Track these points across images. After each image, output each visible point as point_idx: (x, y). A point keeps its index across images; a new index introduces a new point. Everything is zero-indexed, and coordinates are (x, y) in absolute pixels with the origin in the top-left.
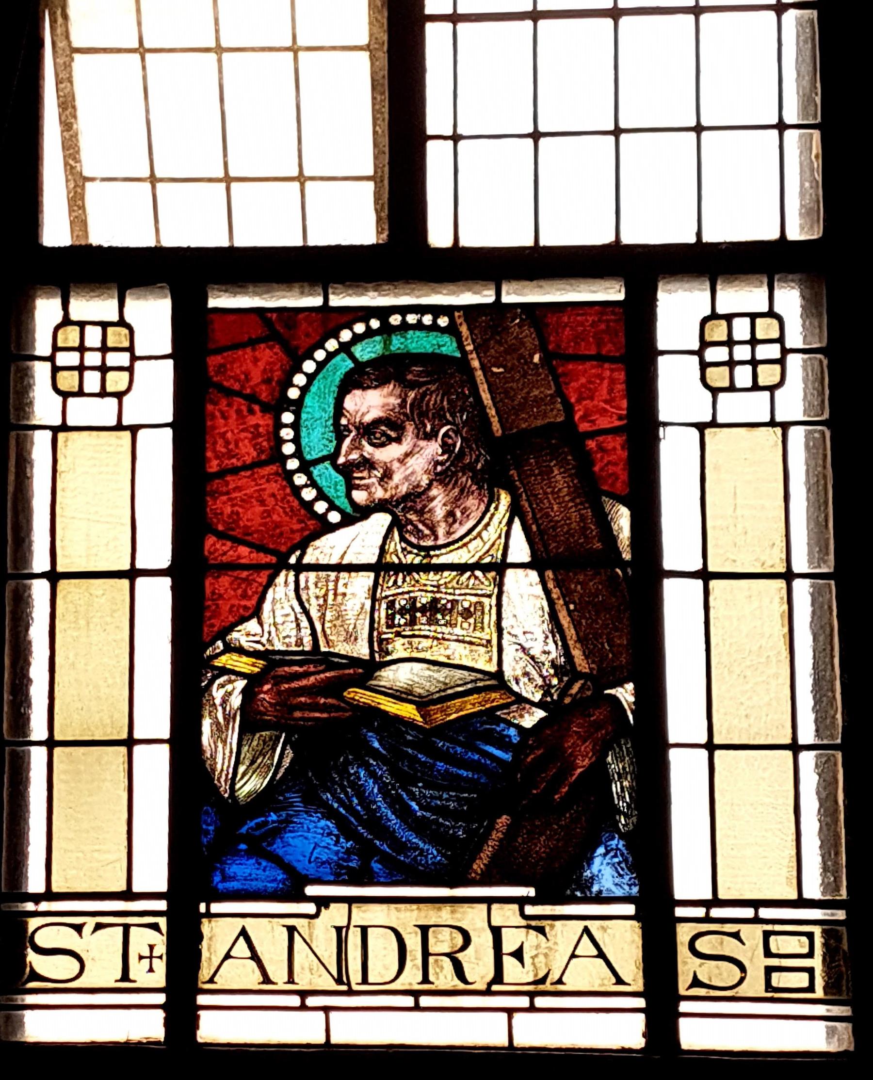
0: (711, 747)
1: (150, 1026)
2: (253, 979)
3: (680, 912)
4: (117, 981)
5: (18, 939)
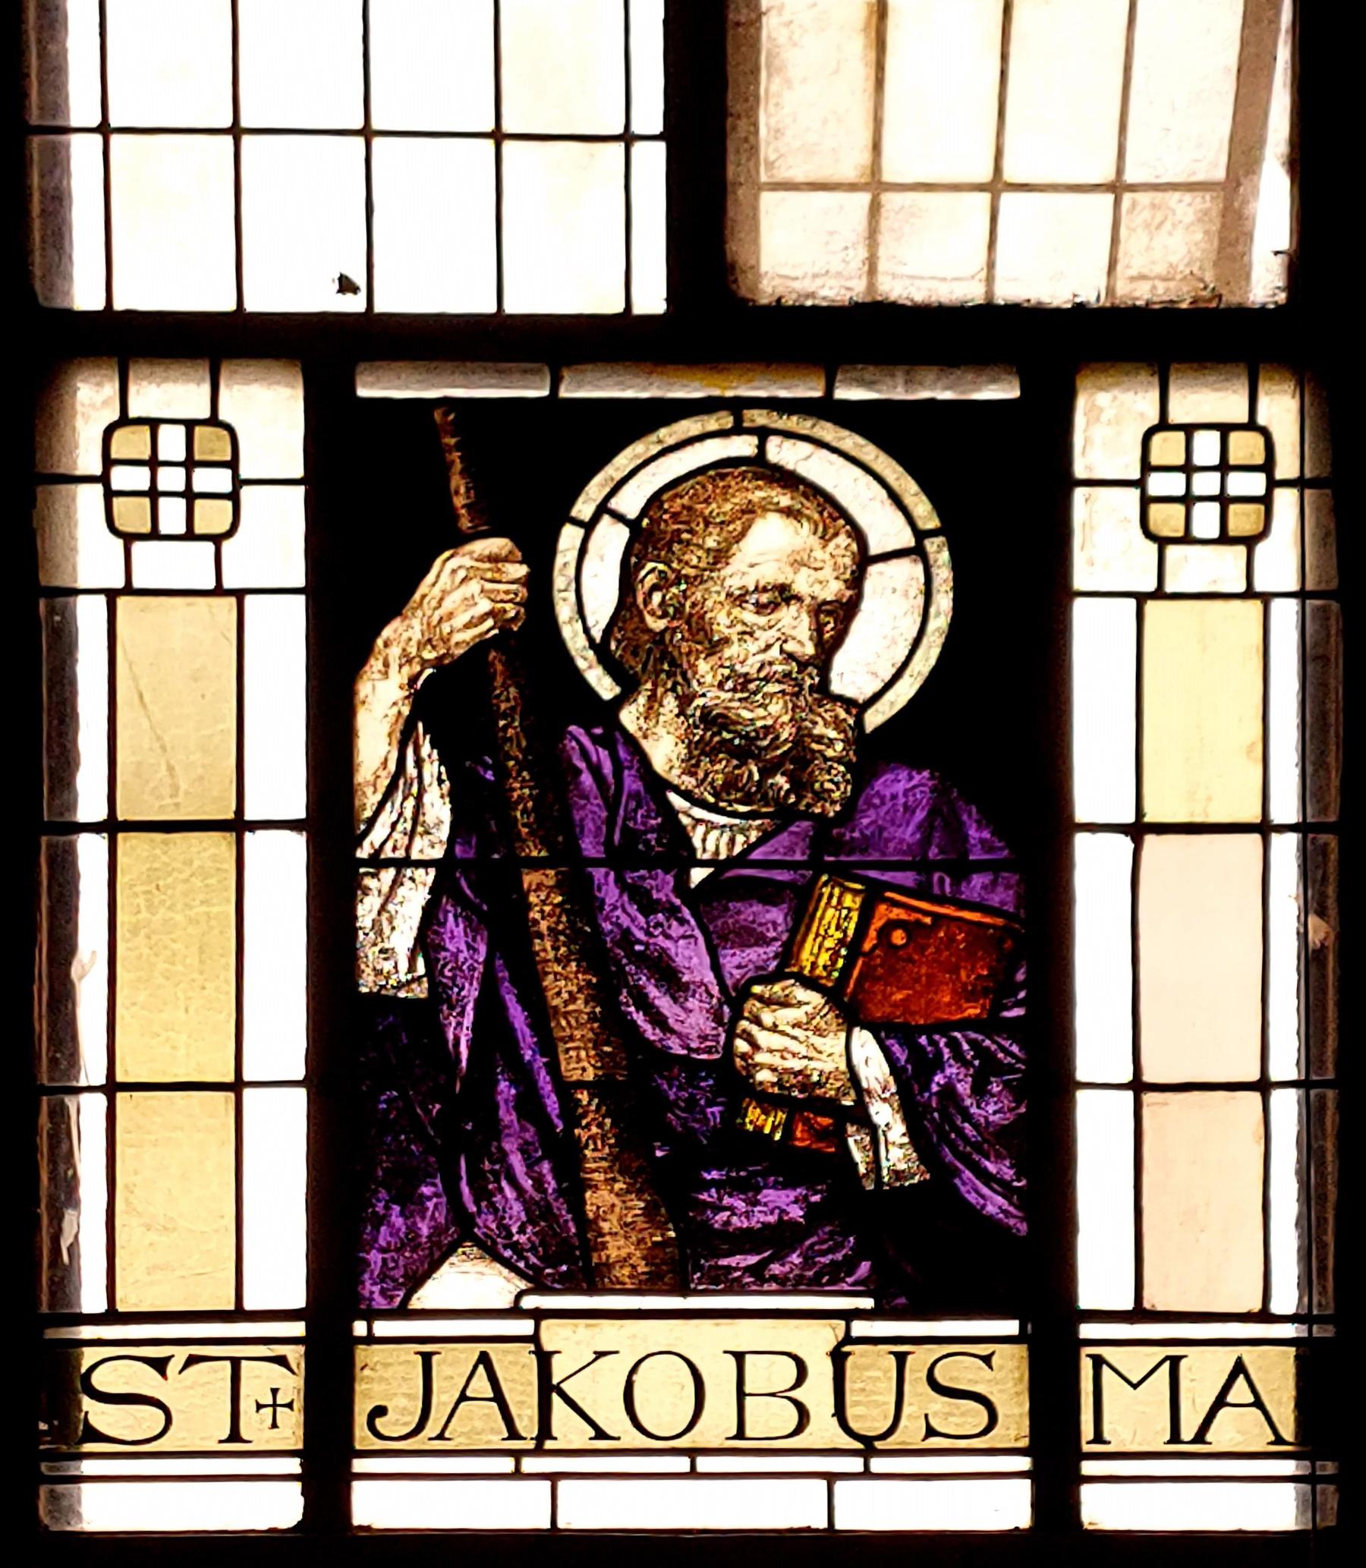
0: (1138, 1086)
1: (279, 1507)
2: (497, 1438)
3: (1087, 1331)
4: (221, 1442)
5: (60, 1382)
